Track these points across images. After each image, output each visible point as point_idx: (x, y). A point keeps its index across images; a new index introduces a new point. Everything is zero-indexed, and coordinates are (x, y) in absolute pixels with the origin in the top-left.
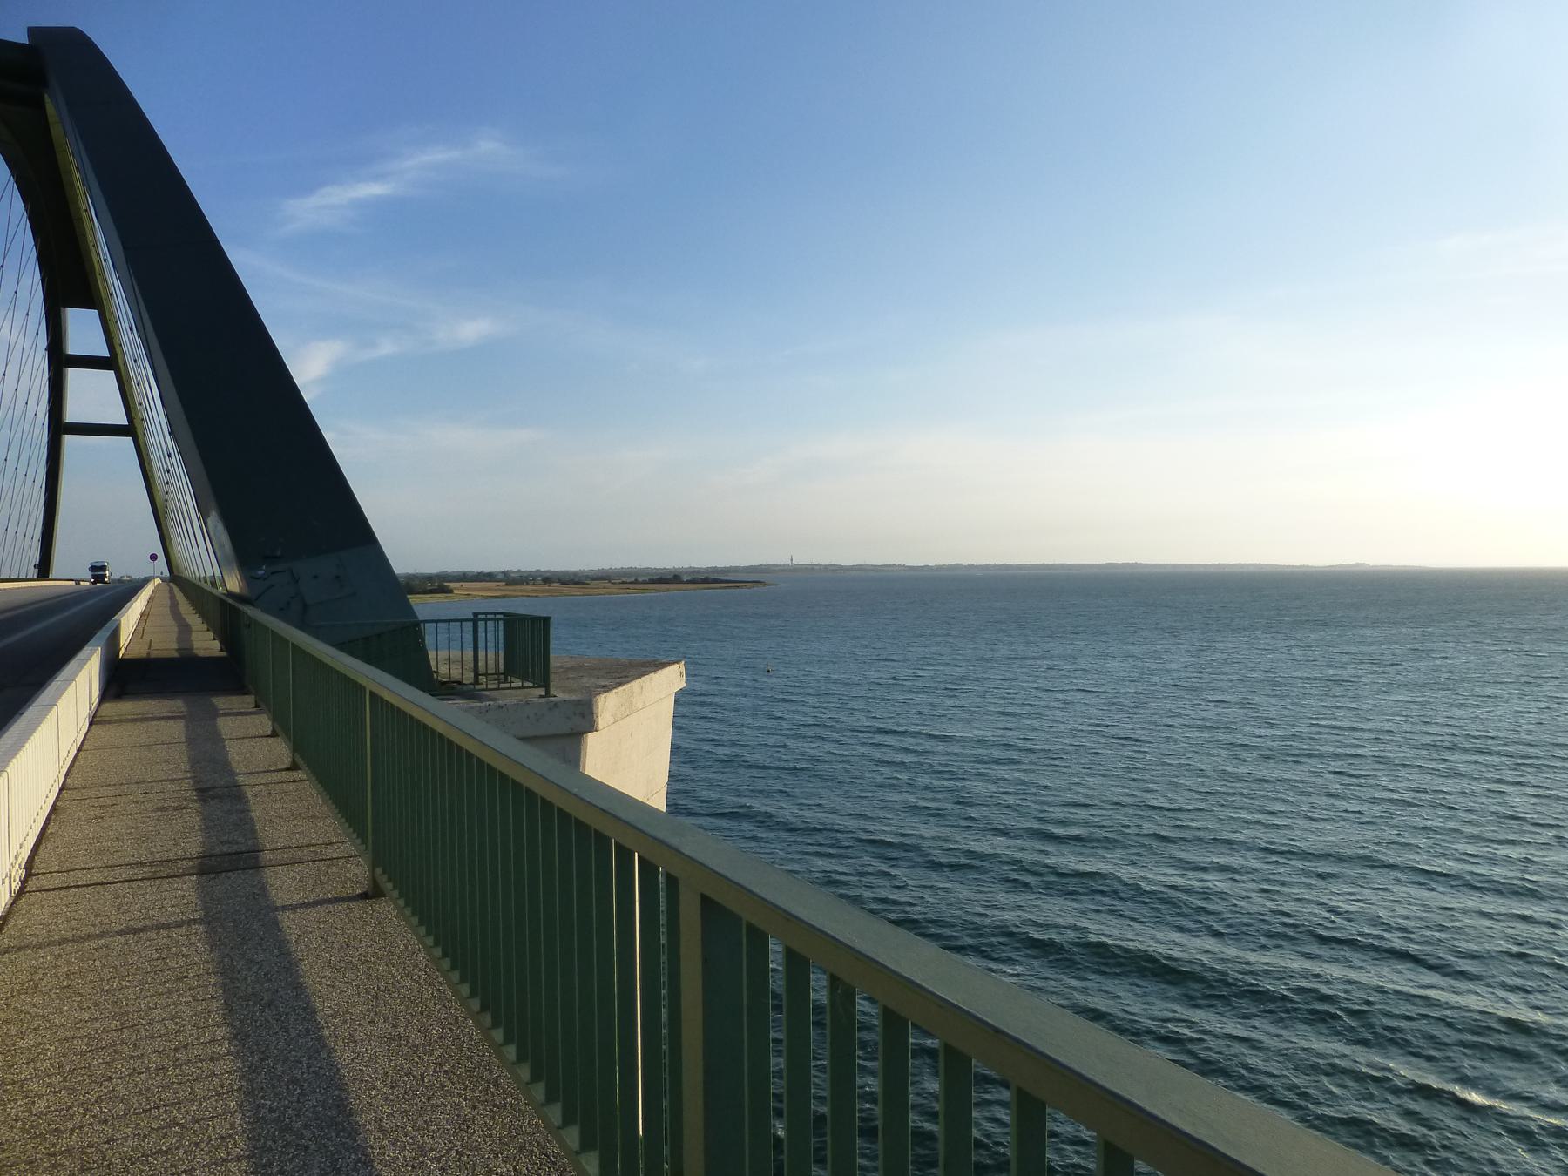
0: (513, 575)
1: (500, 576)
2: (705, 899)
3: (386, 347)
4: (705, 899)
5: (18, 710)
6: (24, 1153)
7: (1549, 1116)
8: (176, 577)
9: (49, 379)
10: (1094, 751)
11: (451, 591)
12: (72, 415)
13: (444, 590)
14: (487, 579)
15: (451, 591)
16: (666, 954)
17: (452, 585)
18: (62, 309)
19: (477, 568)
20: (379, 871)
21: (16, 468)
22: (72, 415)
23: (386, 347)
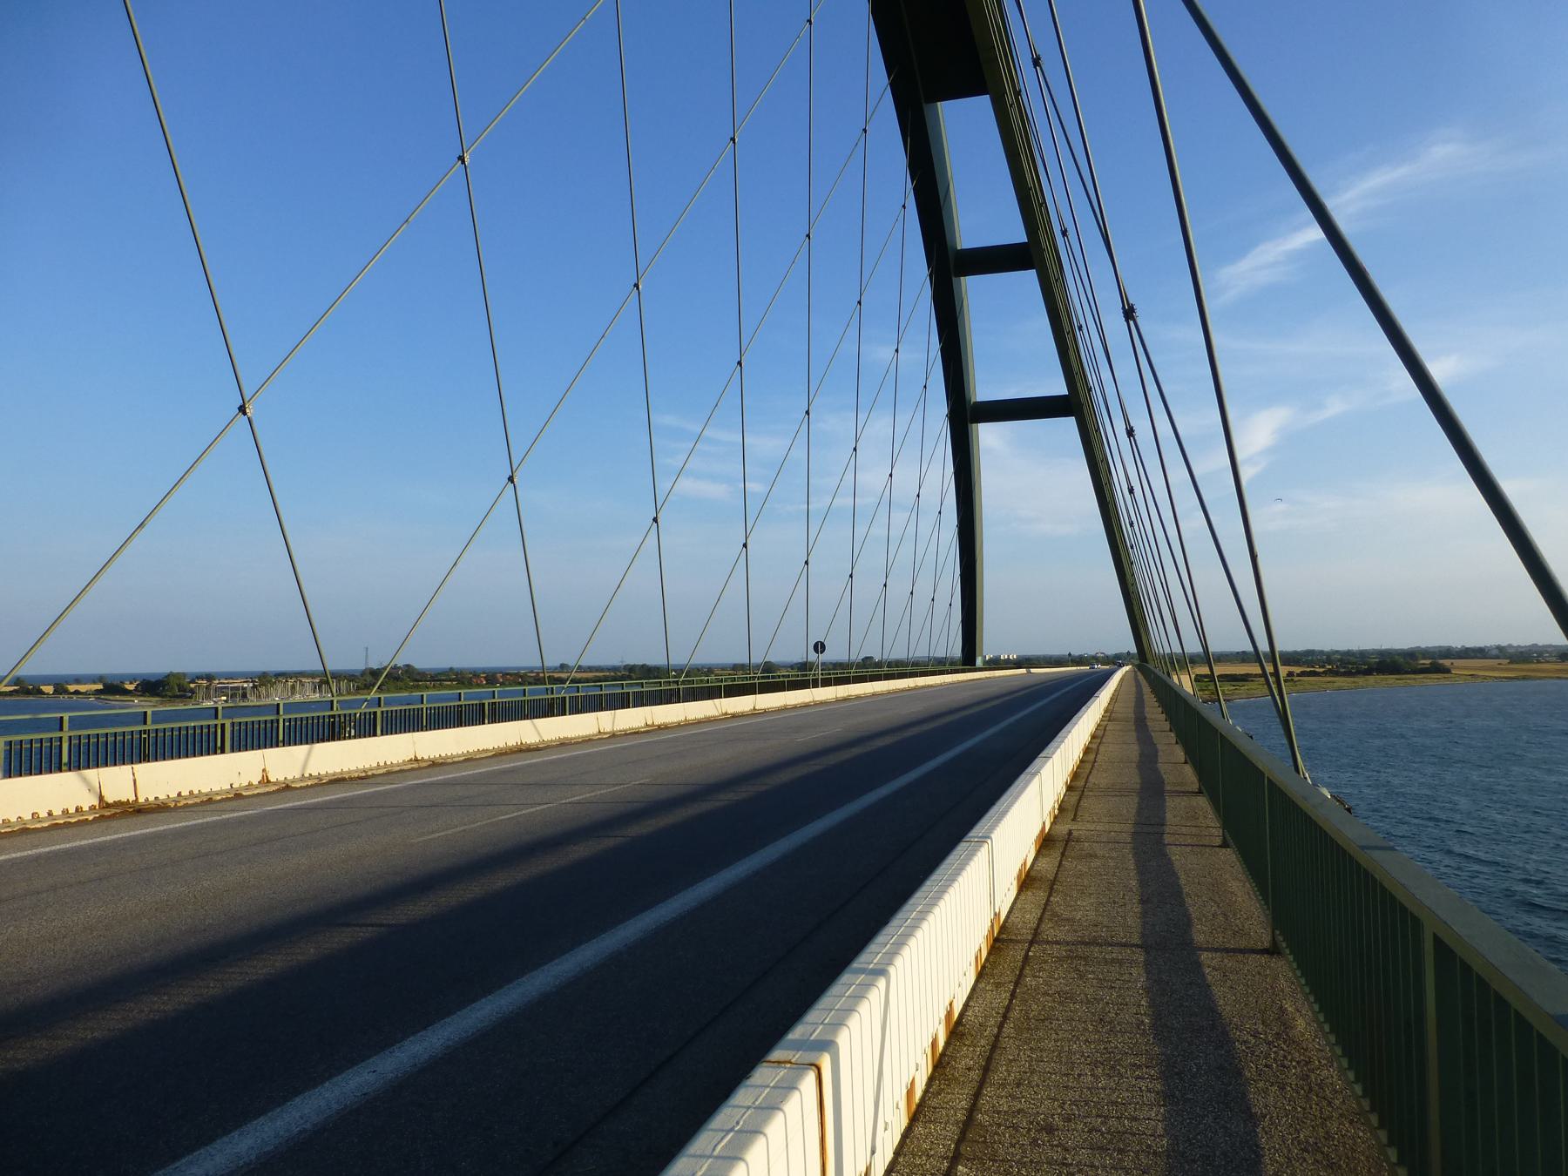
0: (1510, 651)
1: (1495, 652)
2: (1435, 935)
3: (1335, 407)
4: (1435, 935)
5: (963, 838)
6: (991, 1003)
7: (444, 779)
8: (1143, 656)
9: (961, 575)
10: (1432, 850)
11: (1448, 671)
12: (984, 390)
13: (1437, 669)
14: (1479, 655)
15: (1448, 671)
16: (132, 699)
17: (1447, 663)
18: (974, 425)
19: (1471, 643)
20: (1277, 932)
21: (950, 605)
22: (984, 390)
23: (1335, 407)
